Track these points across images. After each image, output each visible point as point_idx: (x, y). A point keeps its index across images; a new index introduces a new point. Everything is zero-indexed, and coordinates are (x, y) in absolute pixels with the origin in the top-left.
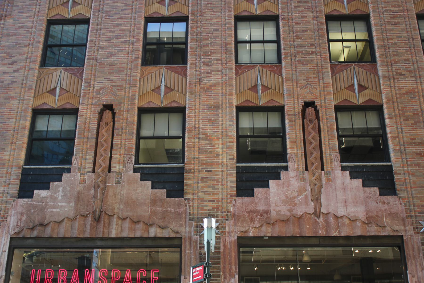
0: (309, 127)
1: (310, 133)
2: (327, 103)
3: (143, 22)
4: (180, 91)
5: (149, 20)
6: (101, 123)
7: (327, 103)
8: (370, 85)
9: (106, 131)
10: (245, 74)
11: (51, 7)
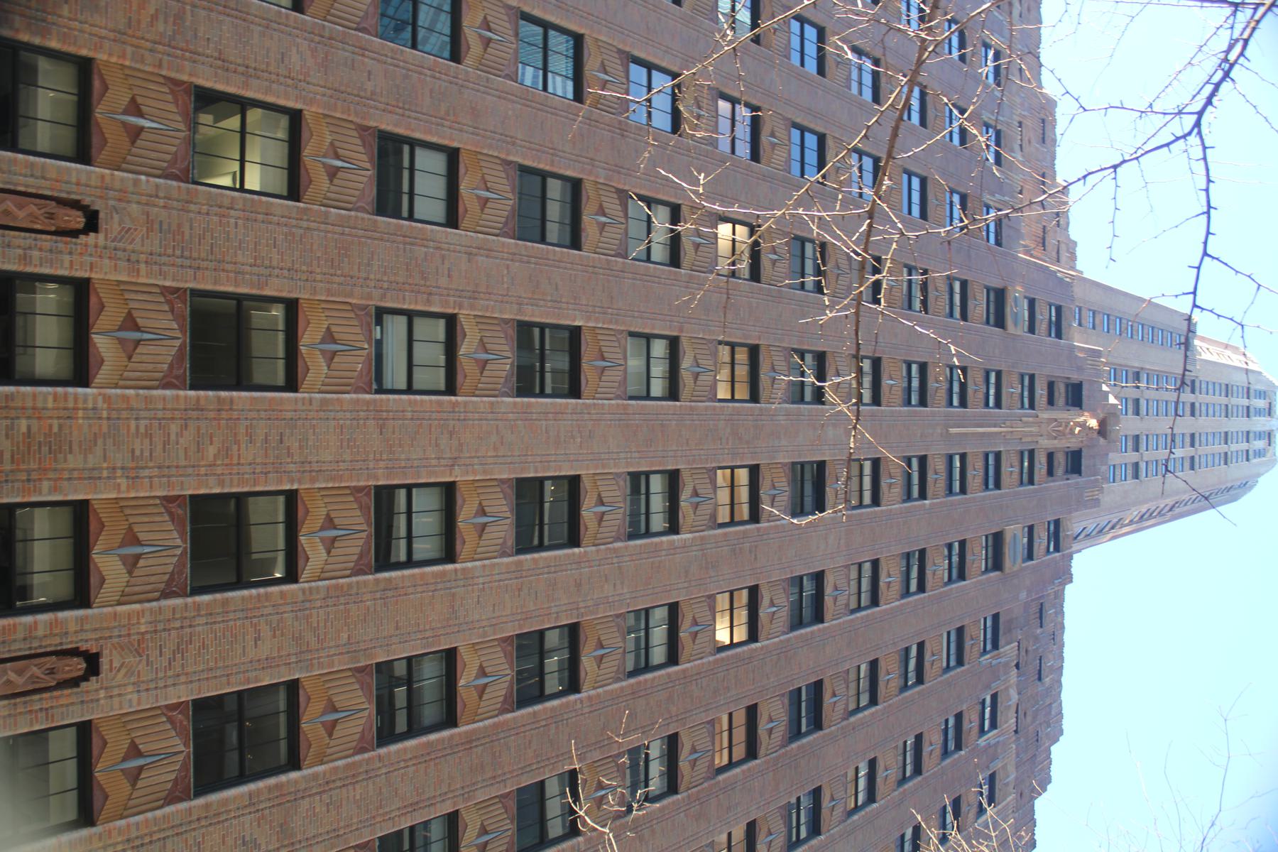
0: (35, 669)
1: (20, 672)
2: (99, 702)
3: (291, 104)
4: (126, 374)
5: (674, 343)
6: (54, 204)
7: (99, 702)
8: (339, 741)
9: (31, 215)
10: (355, 506)
11: (480, 157)
